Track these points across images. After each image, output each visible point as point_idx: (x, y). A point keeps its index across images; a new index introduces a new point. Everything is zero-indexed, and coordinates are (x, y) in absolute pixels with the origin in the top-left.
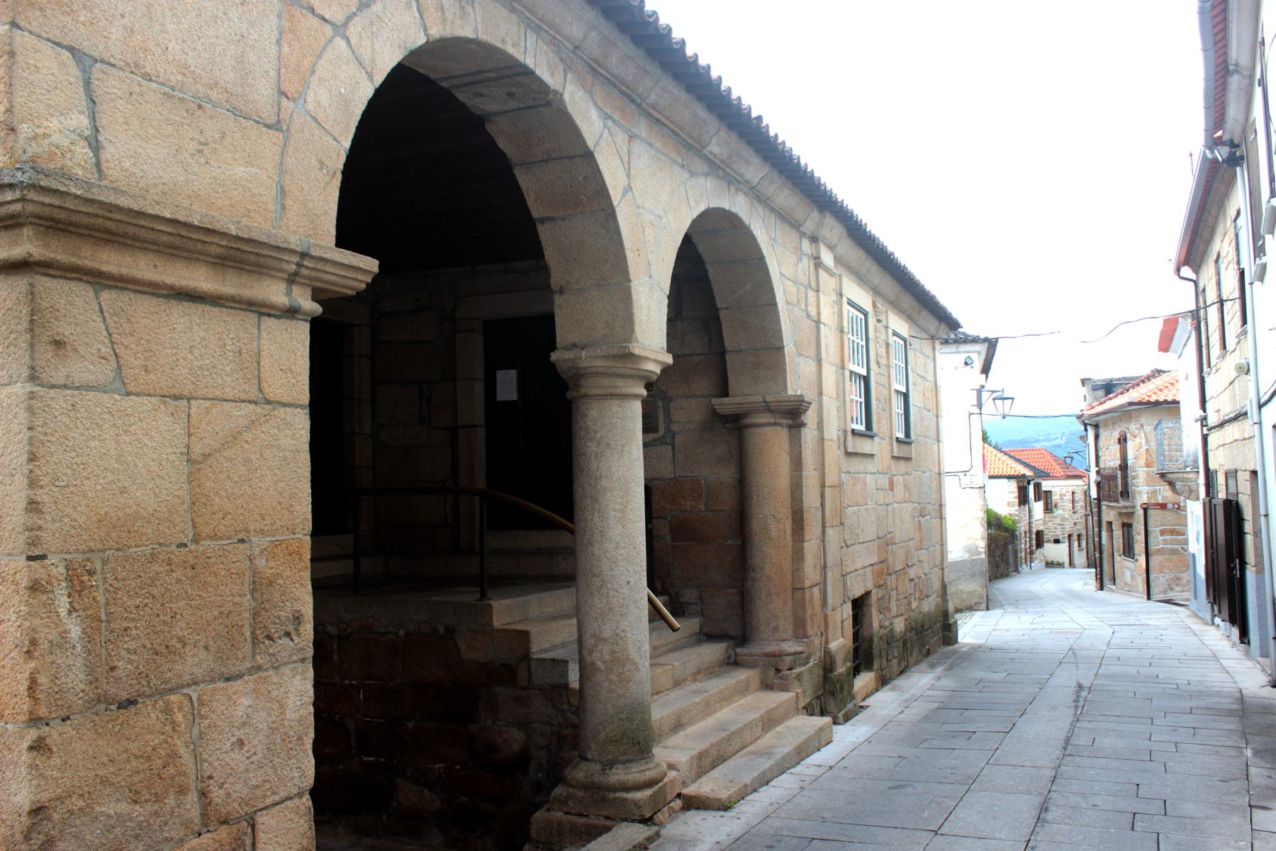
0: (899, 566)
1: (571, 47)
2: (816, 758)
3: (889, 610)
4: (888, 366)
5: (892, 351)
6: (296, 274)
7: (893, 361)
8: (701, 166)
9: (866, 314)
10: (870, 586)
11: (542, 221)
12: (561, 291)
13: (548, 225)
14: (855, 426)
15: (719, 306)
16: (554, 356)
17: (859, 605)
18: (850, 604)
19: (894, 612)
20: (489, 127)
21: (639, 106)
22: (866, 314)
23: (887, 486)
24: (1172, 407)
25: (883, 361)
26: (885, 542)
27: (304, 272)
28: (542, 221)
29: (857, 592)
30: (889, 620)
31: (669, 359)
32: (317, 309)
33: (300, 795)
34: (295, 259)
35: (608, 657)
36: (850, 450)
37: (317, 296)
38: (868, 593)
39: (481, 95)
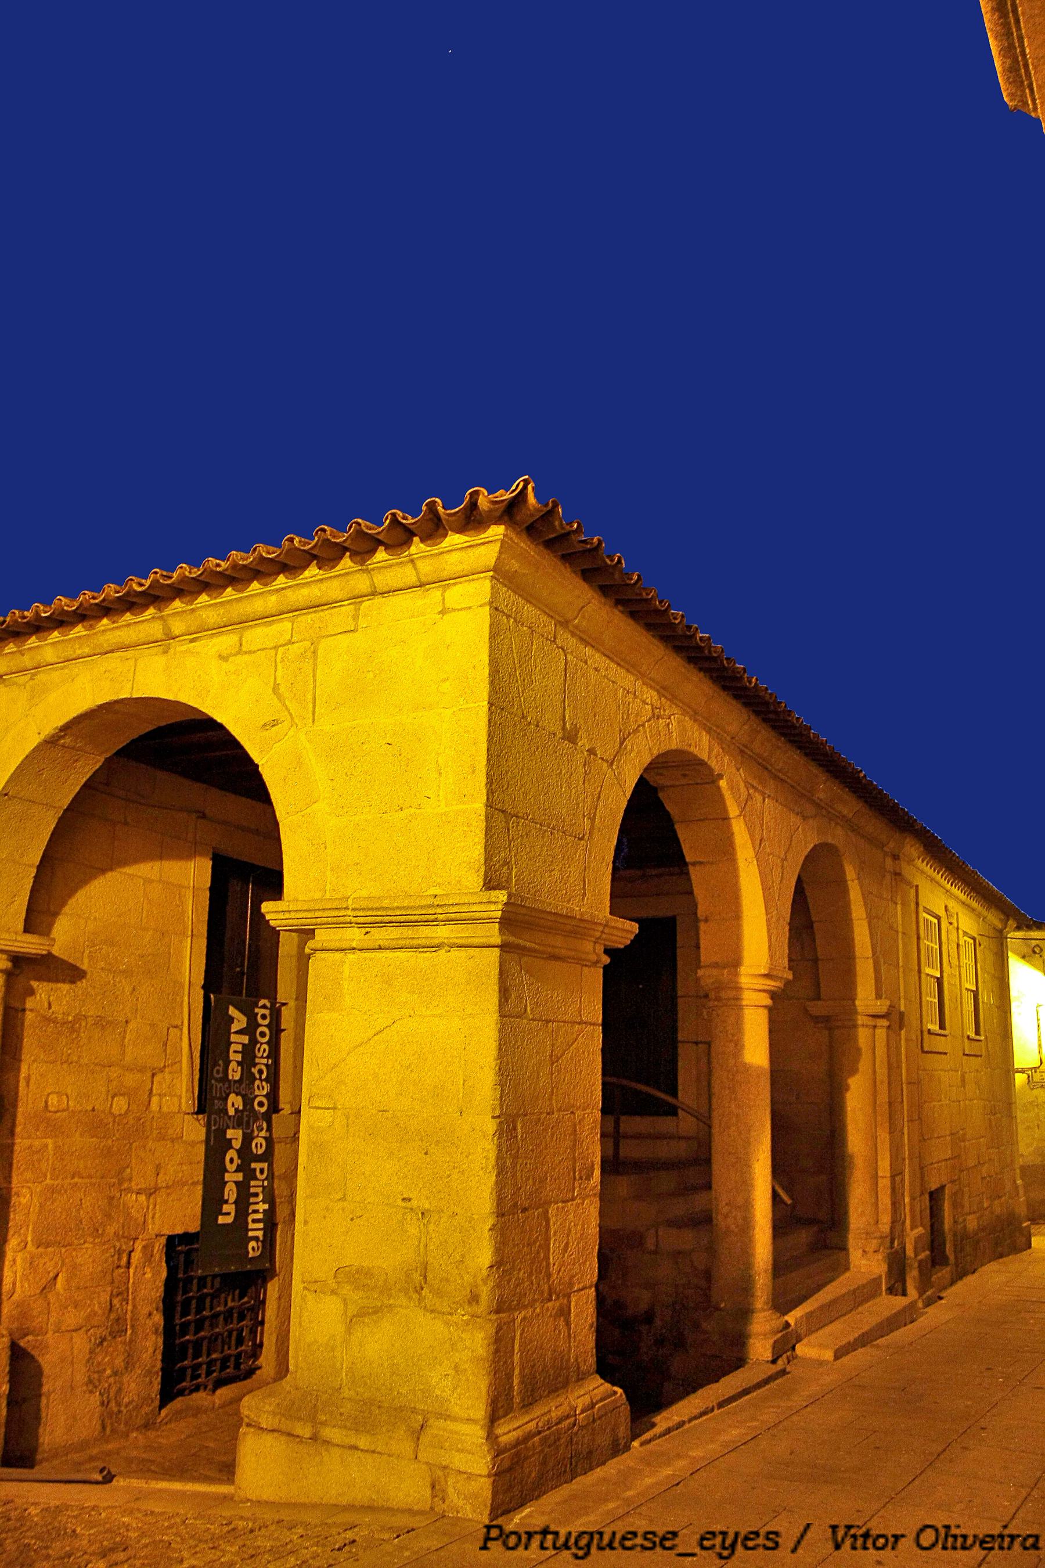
0: (971, 1163)
1: (728, 738)
2: (897, 1334)
3: (963, 1207)
4: (959, 967)
5: (962, 950)
6: (599, 938)
7: (964, 961)
8: (810, 810)
9: (938, 918)
10: (944, 1179)
11: (694, 864)
12: (706, 920)
13: (698, 868)
14: (930, 1026)
15: (813, 919)
16: (700, 973)
17: (935, 1197)
18: (927, 1196)
19: (967, 1209)
20: (661, 795)
21: (770, 771)
22: (938, 918)
23: (959, 1084)
24: (909, 1083)
25: (955, 962)
26: (958, 1138)
27: (604, 936)
28: (694, 864)
29: (933, 1187)
30: (964, 1218)
31: (790, 976)
32: (606, 960)
33: (590, 1287)
34: (601, 928)
35: (741, 1222)
36: (926, 1049)
37: (607, 951)
38: (943, 1187)
39: (661, 774)
